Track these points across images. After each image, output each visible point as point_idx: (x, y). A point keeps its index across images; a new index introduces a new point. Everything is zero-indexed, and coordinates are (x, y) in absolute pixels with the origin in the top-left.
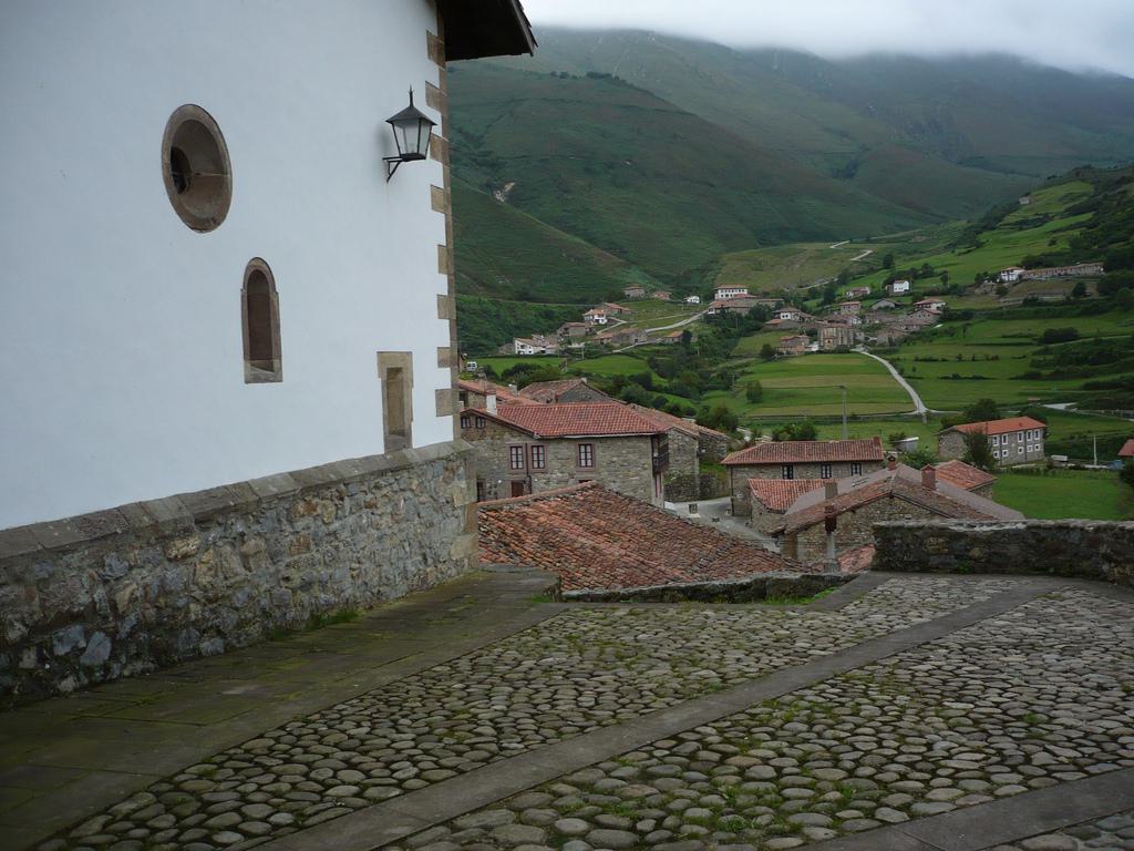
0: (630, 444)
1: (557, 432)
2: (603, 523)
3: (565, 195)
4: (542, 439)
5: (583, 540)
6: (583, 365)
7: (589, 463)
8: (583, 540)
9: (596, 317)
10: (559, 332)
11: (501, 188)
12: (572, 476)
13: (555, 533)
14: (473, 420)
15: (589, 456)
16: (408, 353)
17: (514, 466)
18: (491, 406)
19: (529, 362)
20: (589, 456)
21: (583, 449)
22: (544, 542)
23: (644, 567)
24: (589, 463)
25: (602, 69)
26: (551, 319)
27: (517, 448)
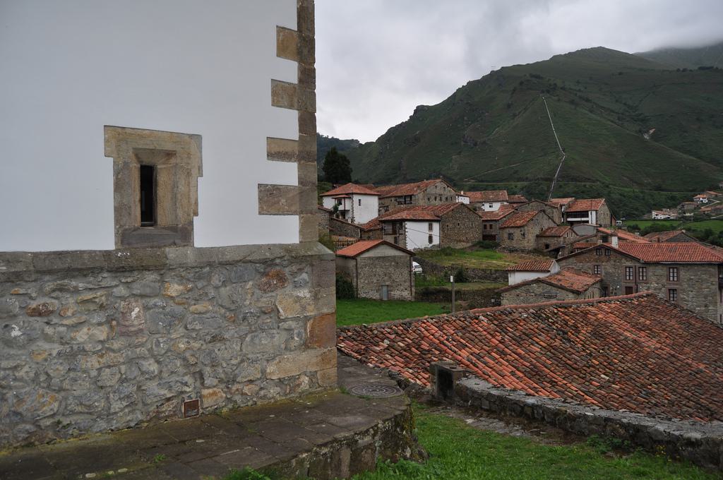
0: (703, 269)
1: (655, 259)
2: (648, 322)
3: (685, 134)
4: (646, 263)
5: (628, 334)
6: (692, 225)
7: (675, 279)
8: (628, 334)
9: (701, 199)
10: (679, 207)
11: (647, 132)
12: (664, 286)
13: (607, 327)
14: (603, 251)
15: (675, 275)
16: (191, 136)
17: (628, 278)
18: (614, 243)
19: (660, 223)
20: (675, 275)
21: (671, 270)
22: (596, 334)
23: (673, 359)
24: (675, 279)
25: (707, 64)
26: (674, 200)
27: (629, 267)
